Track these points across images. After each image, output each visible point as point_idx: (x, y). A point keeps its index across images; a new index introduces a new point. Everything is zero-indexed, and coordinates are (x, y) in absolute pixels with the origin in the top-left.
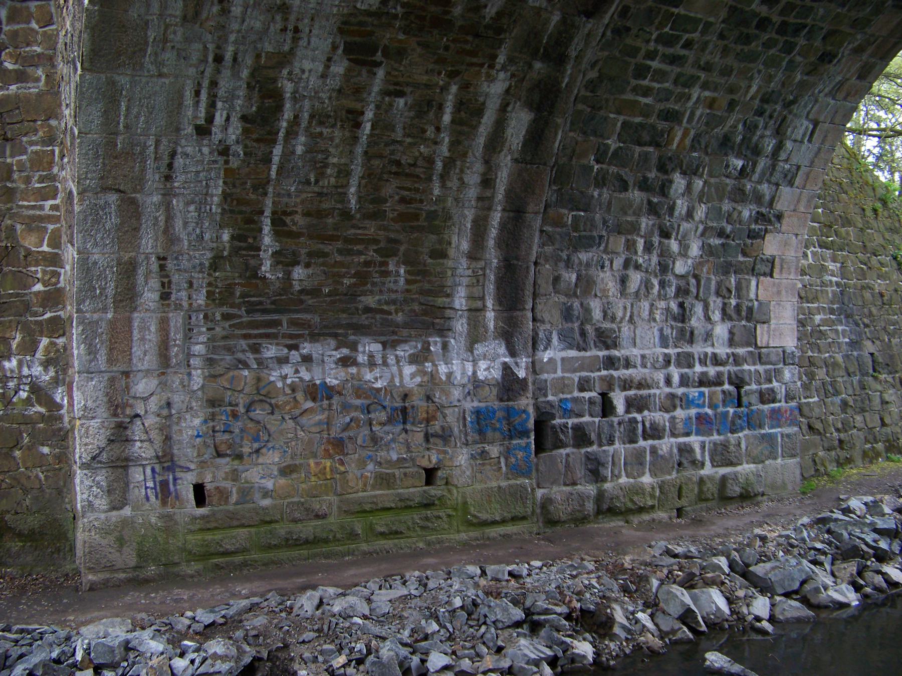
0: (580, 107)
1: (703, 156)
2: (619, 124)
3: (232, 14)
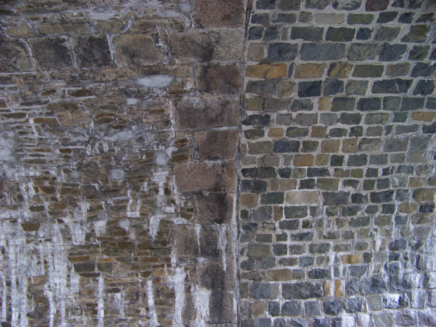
0: (244, 281)
1: (360, 297)
2: (280, 287)
3: (10, 259)
